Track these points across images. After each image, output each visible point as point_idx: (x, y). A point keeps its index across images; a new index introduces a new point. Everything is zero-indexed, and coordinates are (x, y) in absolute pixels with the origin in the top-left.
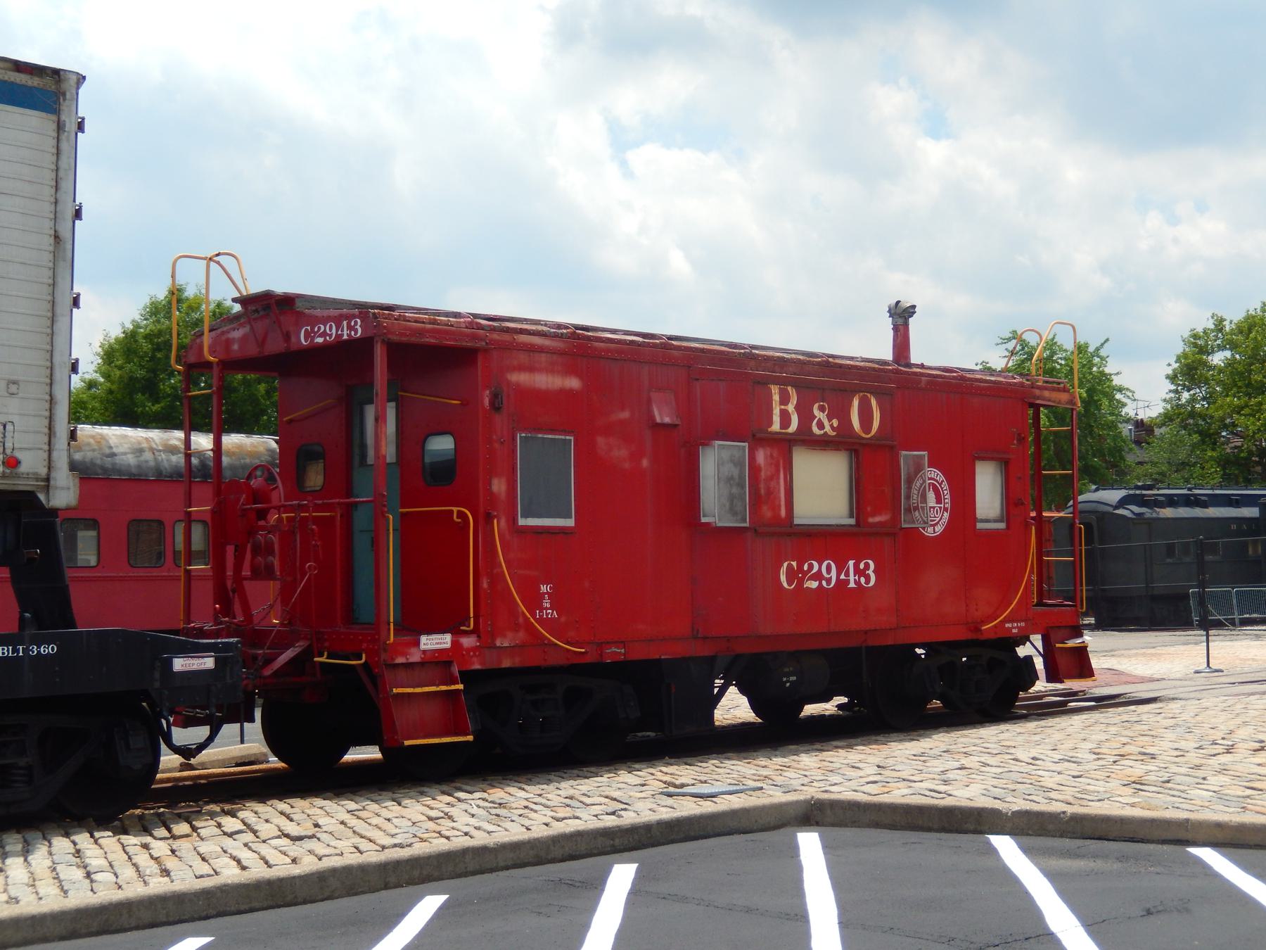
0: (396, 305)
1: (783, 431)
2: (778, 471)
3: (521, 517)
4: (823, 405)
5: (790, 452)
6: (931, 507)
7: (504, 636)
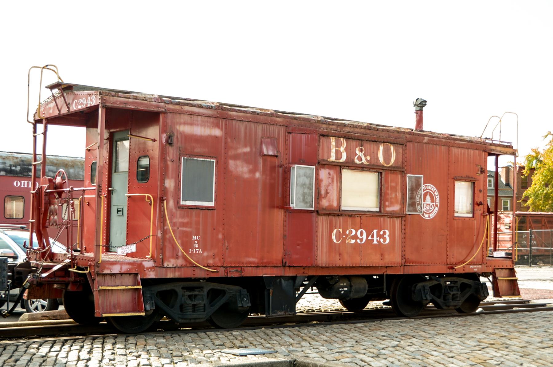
0: (172, 100)
1: (337, 161)
2: (333, 181)
3: (182, 200)
4: (362, 149)
5: (340, 173)
6: (427, 204)
7: (169, 261)
